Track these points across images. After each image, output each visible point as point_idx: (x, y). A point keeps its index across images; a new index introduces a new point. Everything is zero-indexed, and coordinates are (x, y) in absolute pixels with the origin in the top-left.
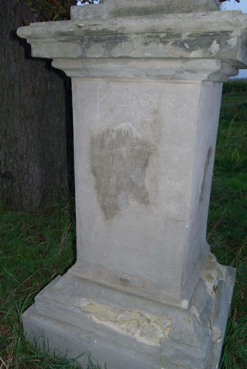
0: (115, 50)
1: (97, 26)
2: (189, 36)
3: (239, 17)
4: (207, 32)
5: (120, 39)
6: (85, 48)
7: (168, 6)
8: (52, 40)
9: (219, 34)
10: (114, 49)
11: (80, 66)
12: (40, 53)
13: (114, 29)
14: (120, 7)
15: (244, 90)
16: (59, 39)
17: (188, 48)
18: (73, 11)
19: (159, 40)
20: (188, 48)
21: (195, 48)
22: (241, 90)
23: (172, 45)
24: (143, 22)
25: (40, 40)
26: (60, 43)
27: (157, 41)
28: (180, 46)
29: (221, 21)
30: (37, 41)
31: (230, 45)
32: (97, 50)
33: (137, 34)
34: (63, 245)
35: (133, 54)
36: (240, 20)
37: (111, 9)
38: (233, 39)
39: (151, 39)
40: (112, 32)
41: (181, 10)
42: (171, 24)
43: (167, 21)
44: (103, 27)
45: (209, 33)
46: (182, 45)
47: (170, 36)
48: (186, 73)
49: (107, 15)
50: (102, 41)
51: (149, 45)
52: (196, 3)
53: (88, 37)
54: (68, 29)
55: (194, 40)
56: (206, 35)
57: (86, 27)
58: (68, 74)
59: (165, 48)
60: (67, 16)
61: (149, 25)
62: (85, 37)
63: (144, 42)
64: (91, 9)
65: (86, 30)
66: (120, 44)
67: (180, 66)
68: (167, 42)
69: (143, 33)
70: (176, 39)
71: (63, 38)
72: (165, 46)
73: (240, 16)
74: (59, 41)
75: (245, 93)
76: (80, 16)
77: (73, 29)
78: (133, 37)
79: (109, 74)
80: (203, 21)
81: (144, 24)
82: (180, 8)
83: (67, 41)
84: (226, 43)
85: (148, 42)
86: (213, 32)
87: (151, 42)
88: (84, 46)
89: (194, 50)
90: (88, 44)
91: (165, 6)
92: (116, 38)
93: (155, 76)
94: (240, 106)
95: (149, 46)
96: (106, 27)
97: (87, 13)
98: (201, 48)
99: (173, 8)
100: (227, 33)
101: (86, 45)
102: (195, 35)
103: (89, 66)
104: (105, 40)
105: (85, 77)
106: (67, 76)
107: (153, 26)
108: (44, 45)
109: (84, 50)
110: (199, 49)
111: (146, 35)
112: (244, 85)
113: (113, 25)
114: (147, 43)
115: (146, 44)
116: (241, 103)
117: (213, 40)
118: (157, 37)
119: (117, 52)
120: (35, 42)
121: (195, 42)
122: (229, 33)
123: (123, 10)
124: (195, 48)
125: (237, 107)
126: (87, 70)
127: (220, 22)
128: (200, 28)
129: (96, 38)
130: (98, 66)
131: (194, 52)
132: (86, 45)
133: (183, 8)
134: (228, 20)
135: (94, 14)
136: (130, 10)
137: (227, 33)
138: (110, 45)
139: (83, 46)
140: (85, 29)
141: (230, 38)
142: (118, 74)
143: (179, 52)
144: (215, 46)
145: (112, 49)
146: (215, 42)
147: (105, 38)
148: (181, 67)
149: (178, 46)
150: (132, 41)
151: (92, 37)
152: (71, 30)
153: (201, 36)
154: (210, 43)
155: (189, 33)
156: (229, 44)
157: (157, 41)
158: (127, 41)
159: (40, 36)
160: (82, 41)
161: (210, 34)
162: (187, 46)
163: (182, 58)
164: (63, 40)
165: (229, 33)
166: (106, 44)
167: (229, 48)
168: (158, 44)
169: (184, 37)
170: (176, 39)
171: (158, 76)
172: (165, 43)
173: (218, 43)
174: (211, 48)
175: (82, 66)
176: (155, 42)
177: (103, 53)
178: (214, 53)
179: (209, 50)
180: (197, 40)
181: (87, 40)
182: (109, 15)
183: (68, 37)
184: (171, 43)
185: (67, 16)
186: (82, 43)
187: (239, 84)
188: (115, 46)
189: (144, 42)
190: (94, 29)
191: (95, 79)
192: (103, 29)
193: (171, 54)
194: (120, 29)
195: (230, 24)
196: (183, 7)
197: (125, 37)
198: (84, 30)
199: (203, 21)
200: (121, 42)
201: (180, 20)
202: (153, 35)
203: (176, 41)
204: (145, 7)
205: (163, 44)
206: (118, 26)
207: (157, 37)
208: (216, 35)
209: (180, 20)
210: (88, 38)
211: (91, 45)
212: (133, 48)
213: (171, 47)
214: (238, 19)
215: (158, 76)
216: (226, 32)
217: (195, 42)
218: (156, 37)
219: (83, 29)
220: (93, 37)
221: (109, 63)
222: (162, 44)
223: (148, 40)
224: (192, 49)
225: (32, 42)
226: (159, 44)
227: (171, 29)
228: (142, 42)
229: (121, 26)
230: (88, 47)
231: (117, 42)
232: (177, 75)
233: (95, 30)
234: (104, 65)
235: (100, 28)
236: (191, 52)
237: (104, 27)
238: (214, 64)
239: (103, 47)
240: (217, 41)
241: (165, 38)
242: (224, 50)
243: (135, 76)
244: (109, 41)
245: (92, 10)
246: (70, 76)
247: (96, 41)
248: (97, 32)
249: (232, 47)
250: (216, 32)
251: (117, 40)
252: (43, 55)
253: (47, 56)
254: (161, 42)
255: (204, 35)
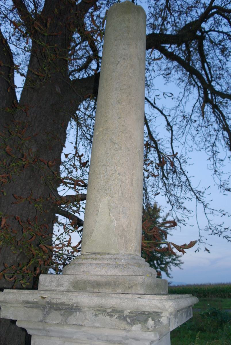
0: (70, 318)
1: (57, 299)
2: (130, 313)
3: (165, 304)
4: (144, 311)
5: (75, 309)
6: (45, 315)
7: (114, 282)
8: (19, 305)
9: (152, 314)
10: (70, 317)
11: (40, 327)
12: (7, 315)
13: (70, 303)
14: (78, 279)
15: (205, 296)
16: (25, 306)
17: (130, 322)
18: (41, 279)
19: (106, 314)
20: (130, 322)
21: (135, 323)
22: (202, 295)
23: (116, 318)
24: (93, 299)
25: (9, 305)
26: (26, 308)
27: (105, 314)
28: (123, 320)
29: (152, 305)
30: (7, 305)
31: (162, 323)
32: (55, 318)
33: (89, 308)
34: (43, 57)
35: (85, 323)
36: (166, 306)
37: (71, 280)
38: (164, 318)
39: (100, 312)
40: (69, 305)
41: (124, 286)
42: (114, 304)
43: (111, 301)
44: (62, 301)
45: (145, 312)
46: (124, 319)
47: (114, 312)
48: (130, 340)
49: (68, 284)
50: (60, 310)
51: (98, 317)
52: (135, 281)
53: (49, 306)
54: (34, 299)
55: (134, 316)
56: (143, 313)
57: (48, 299)
58: (29, 332)
59: (112, 321)
60: (34, 286)
61: (98, 303)
62: (47, 306)
63: (95, 313)
64: (55, 278)
65: (48, 301)
66: (75, 314)
67: (125, 335)
68: (113, 315)
69: (93, 308)
70: (120, 314)
71: (28, 305)
72: (111, 319)
73: (166, 303)
74: (25, 307)
75: (206, 299)
76: (46, 282)
77: (37, 300)
78: (85, 309)
79: (65, 335)
80: (139, 304)
81: (94, 301)
82: (123, 284)
83: (32, 307)
84: (159, 321)
85: (98, 314)
86: (148, 312)
87: (100, 314)
88: (45, 312)
89: (134, 324)
90: (49, 311)
91: (112, 282)
92: (72, 309)
93: (105, 340)
94: (203, 316)
95: (98, 318)
96: (64, 301)
97: (52, 281)
98: (140, 323)
99: (118, 283)
100: (158, 313)
101: (47, 312)
102: (134, 313)
103: (48, 328)
104: (63, 309)
105: (44, 336)
106: (28, 333)
107: (101, 304)
108: (12, 309)
109: (44, 316)
110: (139, 324)
111: (96, 309)
112: (204, 291)
113: (70, 300)
114: (97, 315)
115: (96, 315)
116: (204, 312)
117: (148, 317)
118: (105, 311)
119: (72, 320)
120: (5, 306)
121: (135, 318)
122: (160, 314)
123: (80, 282)
124: (135, 323)
125: (201, 316)
126: (46, 331)
127: (151, 306)
128: (137, 309)
129: (56, 307)
130: (57, 328)
131: (134, 326)
132: (47, 312)
133: (126, 284)
134: (157, 305)
135: (57, 282)
136: (85, 281)
137: (158, 313)
138: (67, 314)
139: (44, 312)
140: (47, 300)
141: (161, 317)
142: (73, 336)
143: (123, 325)
144: (151, 323)
145: (68, 317)
146: (150, 319)
147: (63, 308)
148: (126, 336)
149: (122, 319)
150: (85, 312)
151: (52, 307)
152: (36, 300)
153: (139, 314)
154: (146, 320)
155: (129, 311)
156: (161, 322)
157: (105, 314)
158: (81, 312)
159: (9, 302)
160: (44, 308)
161: (145, 313)
162: (129, 321)
163: (125, 329)
164: (28, 306)
165: (160, 314)
166: (64, 313)
167: (162, 325)
168: (105, 317)
169: (126, 313)
170: (120, 314)
171: (107, 341)
172: (111, 316)
173: (153, 320)
174: (148, 324)
175: (43, 327)
176: (103, 314)
177: (60, 320)
178: (150, 329)
179: (146, 325)
180: (137, 316)
181: (48, 308)
182: (69, 284)
183: (34, 305)
184: (116, 316)
185: (34, 286)
186: (44, 310)
187: (200, 290)
188: (71, 315)
189: (95, 313)
190: (54, 301)
191: (52, 338)
192: (62, 302)
193: (116, 326)
194: (75, 304)
195: (159, 308)
196: (125, 283)
197: (79, 309)
198: (46, 302)
199: (139, 304)
200: (76, 312)
201: (122, 301)
202: (101, 310)
203: (120, 315)
204: (97, 281)
205: (110, 317)
206: (73, 301)
207: (105, 311)
208: (150, 314)
209: (122, 301)
210: (49, 307)
211: (51, 312)
212: (86, 318)
213: (116, 320)
214: (164, 305)
215: (107, 341)
216: (157, 312)
217: (135, 318)
218: (104, 311)
219: (45, 301)
220: (53, 307)
221: (66, 327)
222: (108, 316)
223: (97, 313)
224: (133, 323)
225: (2, 306)
226: (106, 316)
227: (115, 307)
228: (93, 314)
229: (76, 301)
230: (48, 313)
231: (73, 312)
232: (124, 341)
233: (55, 302)
234: (61, 328)
235: (59, 301)
236: (132, 326)
237: (62, 301)
238: (153, 335)
239: (61, 315)
240: (152, 318)
241: (111, 312)
242: (158, 327)
243: (88, 339)
244: (66, 310)
245: (56, 279)
246: (30, 334)
247: (56, 310)
248: (56, 304)
249: (164, 325)
250: (150, 312)
251: (73, 310)
252: (10, 317)
253: (12, 318)
254: (108, 315)
255: (141, 314)
